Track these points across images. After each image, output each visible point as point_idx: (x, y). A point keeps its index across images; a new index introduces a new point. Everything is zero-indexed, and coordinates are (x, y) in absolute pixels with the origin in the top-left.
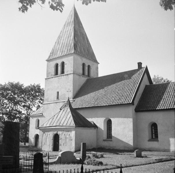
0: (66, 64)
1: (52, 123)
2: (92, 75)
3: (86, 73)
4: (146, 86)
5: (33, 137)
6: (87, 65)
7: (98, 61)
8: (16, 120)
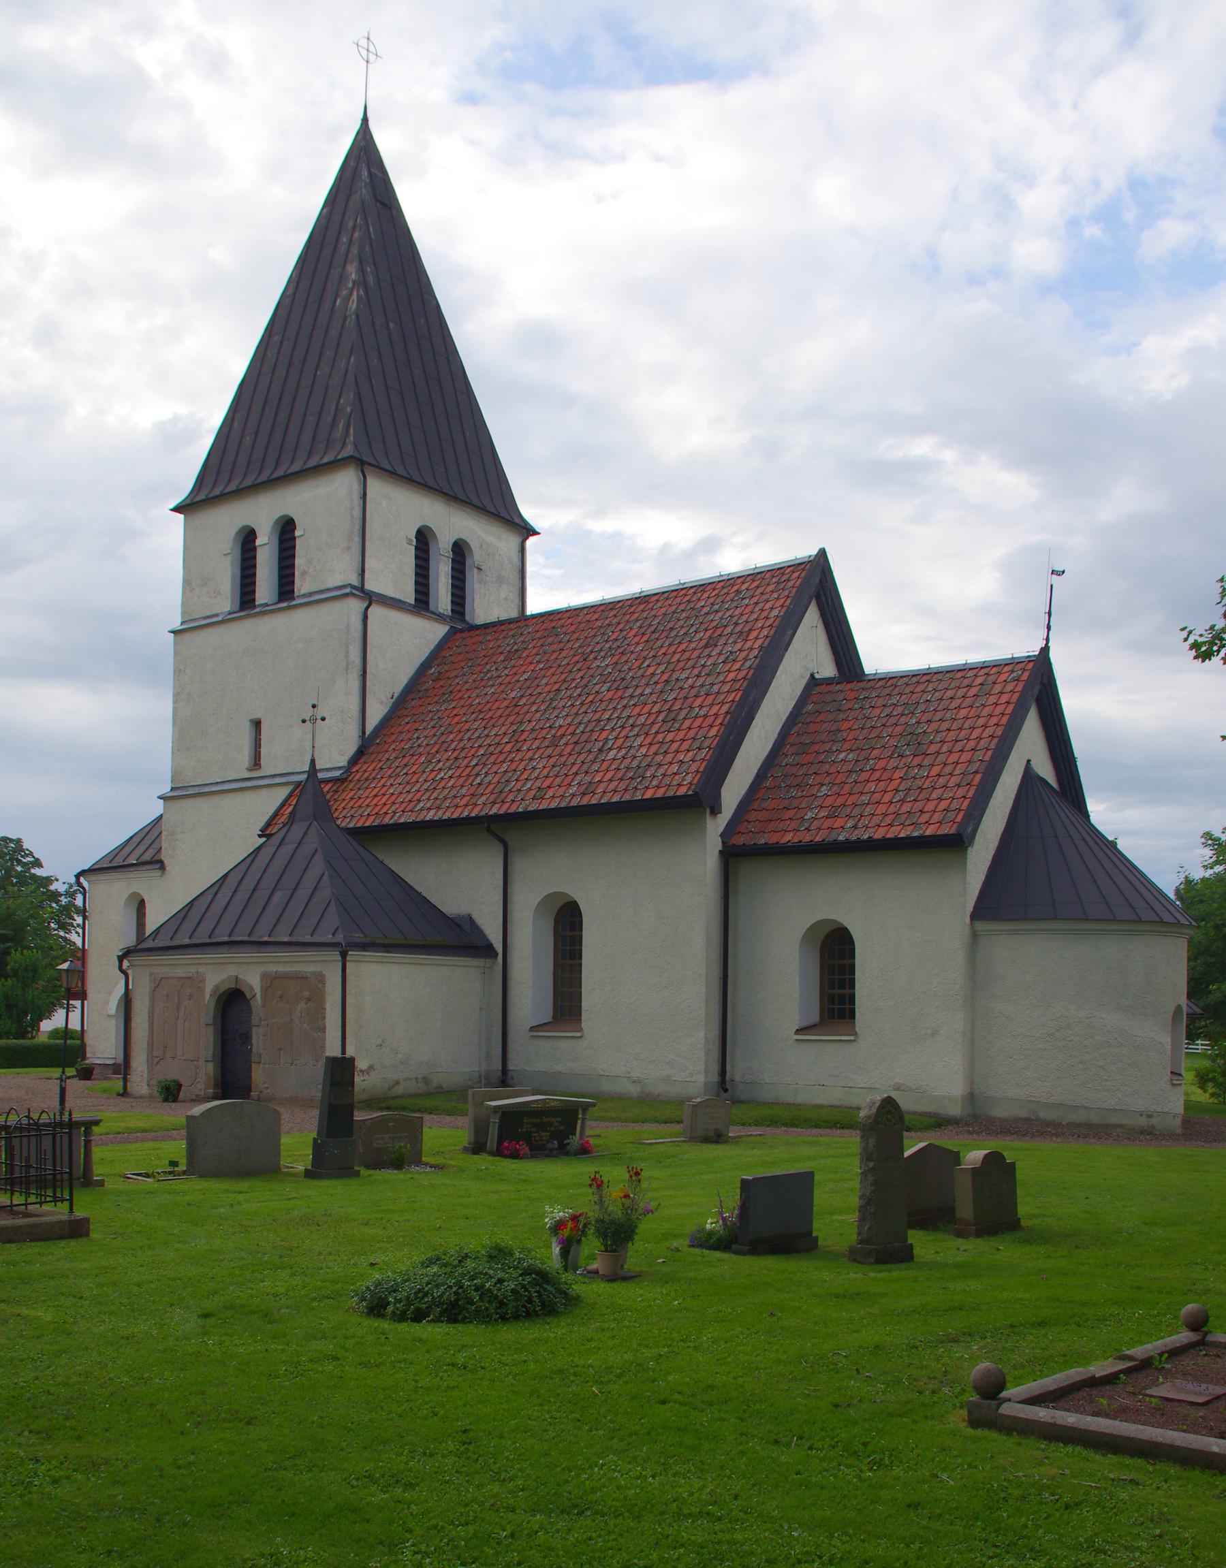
0: (304, 573)
1: (246, 881)
2: (487, 606)
3: (442, 599)
4: (813, 682)
5: (113, 1012)
6: (444, 543)
7: (528, 512)
8: (60, 1015)
